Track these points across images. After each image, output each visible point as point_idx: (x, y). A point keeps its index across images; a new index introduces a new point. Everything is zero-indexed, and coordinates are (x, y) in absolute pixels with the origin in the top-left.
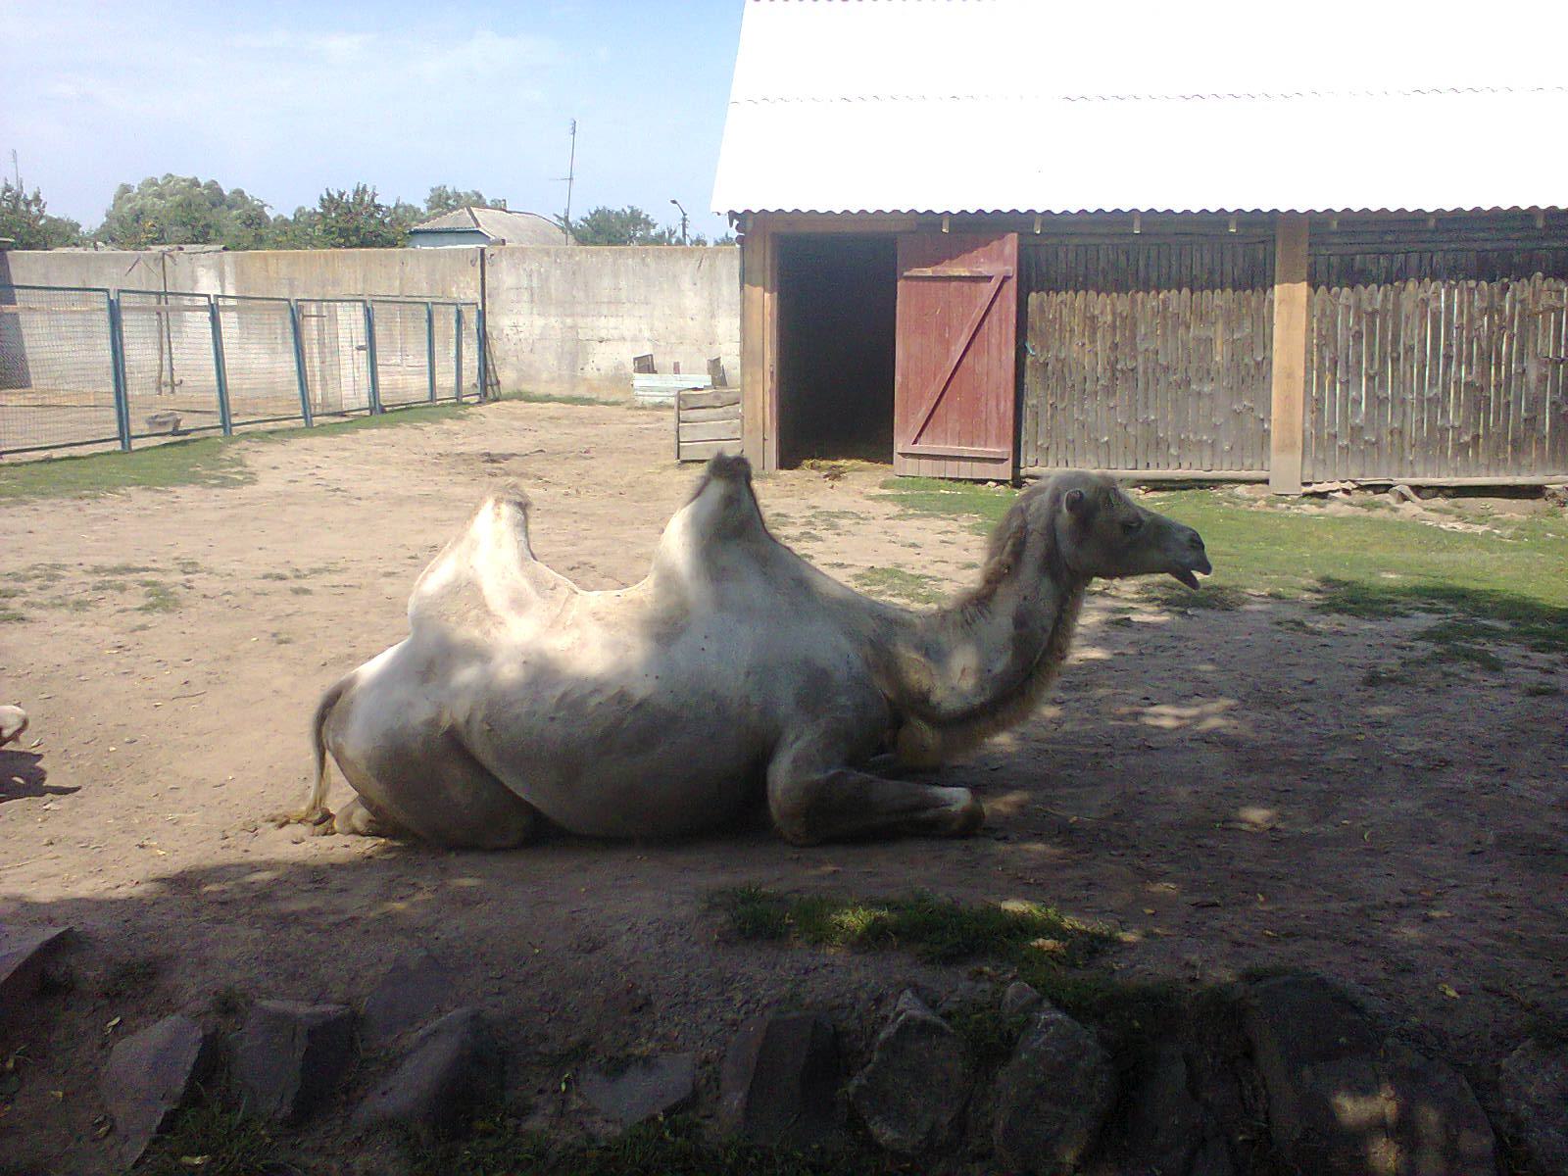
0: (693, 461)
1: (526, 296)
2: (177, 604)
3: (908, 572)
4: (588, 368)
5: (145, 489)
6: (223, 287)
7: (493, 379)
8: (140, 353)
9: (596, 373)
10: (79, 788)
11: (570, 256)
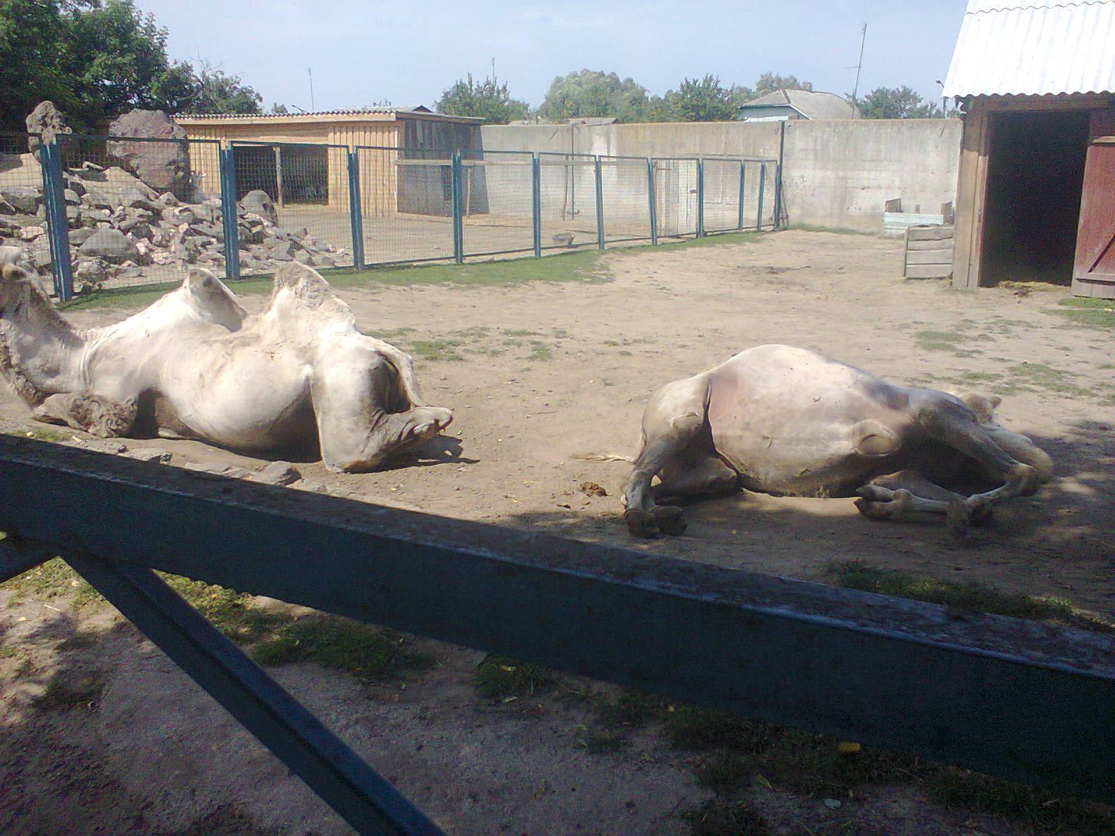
0: (915, 279)
1: (811, 156)
2: (549, 356)
3: (1053, 368)
4: (852, 208)
5: (544, 283)
6: (608, 151)
7: (784, 214)
8: (552, 190)
9: (858, 212)
10: (479, 461)
11: (846, 127)
